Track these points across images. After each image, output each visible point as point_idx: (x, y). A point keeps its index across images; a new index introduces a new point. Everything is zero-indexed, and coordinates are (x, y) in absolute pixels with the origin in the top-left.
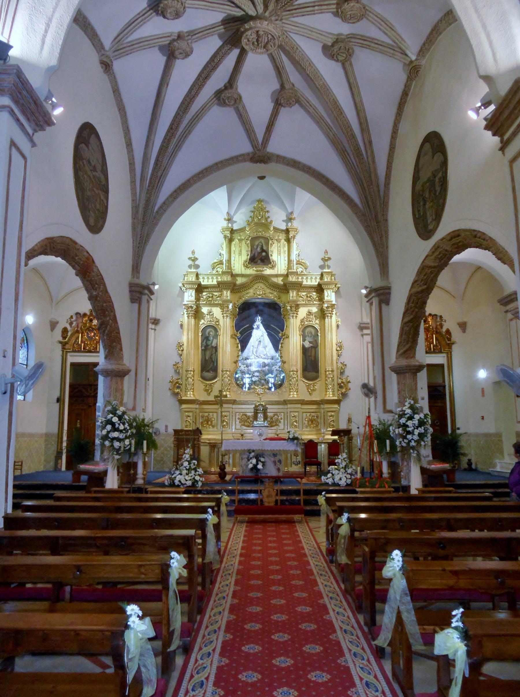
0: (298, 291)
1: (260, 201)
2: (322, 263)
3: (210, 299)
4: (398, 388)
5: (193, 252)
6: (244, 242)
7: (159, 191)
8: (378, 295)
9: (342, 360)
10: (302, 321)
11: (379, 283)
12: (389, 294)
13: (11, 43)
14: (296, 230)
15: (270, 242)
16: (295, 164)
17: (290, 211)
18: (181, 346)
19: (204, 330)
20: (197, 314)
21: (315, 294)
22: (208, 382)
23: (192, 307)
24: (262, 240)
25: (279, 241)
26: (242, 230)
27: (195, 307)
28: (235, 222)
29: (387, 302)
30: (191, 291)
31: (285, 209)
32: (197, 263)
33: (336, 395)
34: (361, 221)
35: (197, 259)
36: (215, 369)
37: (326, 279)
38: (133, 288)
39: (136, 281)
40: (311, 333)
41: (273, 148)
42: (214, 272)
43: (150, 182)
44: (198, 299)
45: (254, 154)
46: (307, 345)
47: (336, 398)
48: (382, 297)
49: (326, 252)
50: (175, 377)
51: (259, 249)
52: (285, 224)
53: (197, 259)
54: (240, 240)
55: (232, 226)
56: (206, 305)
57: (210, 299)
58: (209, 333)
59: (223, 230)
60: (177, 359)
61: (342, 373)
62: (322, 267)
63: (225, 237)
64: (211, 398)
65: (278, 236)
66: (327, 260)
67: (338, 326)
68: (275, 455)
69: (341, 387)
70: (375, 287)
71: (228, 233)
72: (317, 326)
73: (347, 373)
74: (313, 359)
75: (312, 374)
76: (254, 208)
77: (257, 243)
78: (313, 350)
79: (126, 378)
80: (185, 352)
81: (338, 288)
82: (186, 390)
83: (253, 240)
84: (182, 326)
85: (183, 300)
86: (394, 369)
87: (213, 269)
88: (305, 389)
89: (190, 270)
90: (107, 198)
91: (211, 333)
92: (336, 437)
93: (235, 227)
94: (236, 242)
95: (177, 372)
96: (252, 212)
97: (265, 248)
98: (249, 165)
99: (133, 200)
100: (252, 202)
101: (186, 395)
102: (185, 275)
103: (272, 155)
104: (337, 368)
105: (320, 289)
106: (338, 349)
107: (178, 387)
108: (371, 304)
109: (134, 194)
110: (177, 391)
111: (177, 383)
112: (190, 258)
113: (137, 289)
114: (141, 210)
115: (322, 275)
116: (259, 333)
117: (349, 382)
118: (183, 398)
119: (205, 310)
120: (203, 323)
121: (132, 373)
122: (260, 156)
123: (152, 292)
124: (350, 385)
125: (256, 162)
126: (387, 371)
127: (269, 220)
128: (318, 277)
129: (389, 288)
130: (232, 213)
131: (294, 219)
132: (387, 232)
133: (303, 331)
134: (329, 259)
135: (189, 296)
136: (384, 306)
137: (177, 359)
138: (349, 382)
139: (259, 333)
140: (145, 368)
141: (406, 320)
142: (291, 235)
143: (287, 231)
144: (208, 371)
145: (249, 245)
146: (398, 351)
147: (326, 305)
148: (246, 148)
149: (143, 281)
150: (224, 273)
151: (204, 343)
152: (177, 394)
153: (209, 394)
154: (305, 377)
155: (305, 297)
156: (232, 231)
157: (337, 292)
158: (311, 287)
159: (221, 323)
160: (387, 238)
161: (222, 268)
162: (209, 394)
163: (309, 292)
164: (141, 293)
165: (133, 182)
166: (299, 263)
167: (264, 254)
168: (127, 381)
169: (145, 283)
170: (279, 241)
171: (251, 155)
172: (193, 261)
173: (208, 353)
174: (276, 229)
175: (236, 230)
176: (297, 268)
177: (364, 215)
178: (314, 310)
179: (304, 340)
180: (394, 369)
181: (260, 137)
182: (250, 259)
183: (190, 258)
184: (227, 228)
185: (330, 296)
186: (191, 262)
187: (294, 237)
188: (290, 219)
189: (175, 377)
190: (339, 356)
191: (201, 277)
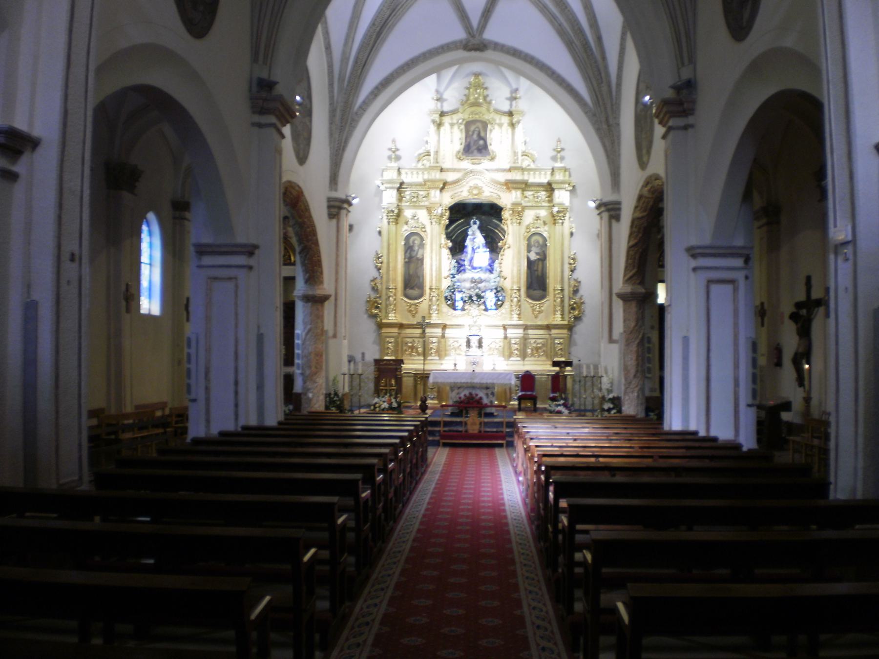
0: (523, 190)
1: (477, 75)
2: (554, 153)
3: (415, 199)
4: (624, 317)
5: (394, 141)
6: (456, 127)
7: (358, 97)
8: (608, 210)
9: (576, 275)
10: (528, 227)
11: (610, 197)
12: (619, 209)
13: (274, 78)
14: (522, 113)
15: (489, 127)
16: (515, 53)
17: (514, 87)
18: (379, 258)
19: (407, 238)
20: (397, 216)
21: (544, 193)
22: (412, 302)
23: (393, 211)
24: (479, 124)
25: (501, 125)
26: (454, 112)
27: (396, 211)
28: (446, 100)
29: (617, 218)
30: (391, 190)
31: (508, 83)
32: (397, 153)
33: (567, 318)
34: (591, 120)
35: (397, 150)
36: (421, 287)
37: (559, 177)
38: (332, 203)
39: (334, 195)
40: (538, 242)
41: (491, 34)
42: (420, 165)
43: (349, 82)
44: (400, 199)
45: (468, 41)
46: (533, 256)
47: (566, 322)
48: (612, 213)
49: (559, 141)
50: (373, 295)
51: (475, 136)
52: (508, 102)
53: (397, 150)
54: (452, 125)
55: (442, 106)
56: (409, 207)
57: (415, 199)
58: (413, 242)
59: (431, 113)
60: (374, 273)
61: (576, 292)
62: (554, 159)
63: (434, 122)
64: (414, 322)
65: (500, 119)
66: (559, 152)
67: (572, 234)
68: (487, 388)
69: (573, 309)
70: (606, 200)
71: (436, 117)
72: (545, 234)
73: (582, 292)
74: (540, 274)
75: (538, 293)
76: (470, 83)
77: (473, 128)
78: (540, 263)
79: (326, 303)
80: (384, 265)
81: (574, 187)
82: (387, 313)
83: (468, 124)
84: (380, 233)
85: (381, 201)
86: (621, 296)
87: (419, 161)
88: (530, 310)
89: (390, 165)
90: (311, 121)
91: (416, 242)
92: (557, 369)
93: (447, 108)
94: (446, 128)
95: (375, 289)
96: (468, 88)
97: (482, 134)
98: (461, 54)
99: (330, 104)
100: (468, 75)
101: (387, 317)
102: (383, 170)
103: (490, 42)
104: (569, 286)
105: (549, 188)
106: (572, 261)
107: (377, 308)
108: (601, 218)
109: (331, 97)
110: (375, 311)
111: (376, 302)
112: (390, 149)
113: (337, 204)
114: (338, 113)
115: (553, 170)
116: (475, 239)
117: (583, 303)
118: (384, 321)
119: (408, 213)
120: (405, 230)
121: (332, 299)
122: (475, 44)
123: (350, 204)
124: (583, 306)
125: (470, 50)
126: (615, 298)
127: (488, 99)
128: (549, 172)
129: (619, 203)
130: (442, 89)
131: (520, 98)
132: (619, 137)
133: (529, 239)
134: (563, 149)
135: (390, 198)
136: (614, 223)
137: (374, 273)
138: (583, 303)
139: (475, 239)
140: (91, 50)
141: (632, 243)
142: (515, 120)
143: (510, 114)
144: (412, 288)
145: (464, 131)
146: (625, 276)
147: (556, 209)
148: (459, 34)
149: (340, 195)
150: (432, 168)
151: (408, 255)
152: (375, 316)
153: (414, 316)
154: (529, 296)
155: (531, 197)
156: (442, 114)
157: (573, 191)
158: (540, 185)
159: (428, 229)
160: (619, 144)
161: (429, 160)
162: (414, 316)
163: (538, 191)
164: (340, 208)
165: (331, 85)
166: (524, 154)
167: (481, 142)
168: (328, 306)
169: (343, 197)
170: (501, 125)
171: (464, 42)
172: (394, 152)
173: (412, 266)
174: (497, 111)
175: (447, 113)
176: (523, 160)
177: (594, 115)
178: (543, 213)
179: (529, 251)
180: (621, 296)
181: (475, 21)
182: (464, 149)
183: (390, 149)
184: (435, 112)
185: (562, 197)
186: (390, 153)
187: (519, 122)
188: (513, 99)
189: (373, 295)
190: (572, 271)
191: (403, 172)
